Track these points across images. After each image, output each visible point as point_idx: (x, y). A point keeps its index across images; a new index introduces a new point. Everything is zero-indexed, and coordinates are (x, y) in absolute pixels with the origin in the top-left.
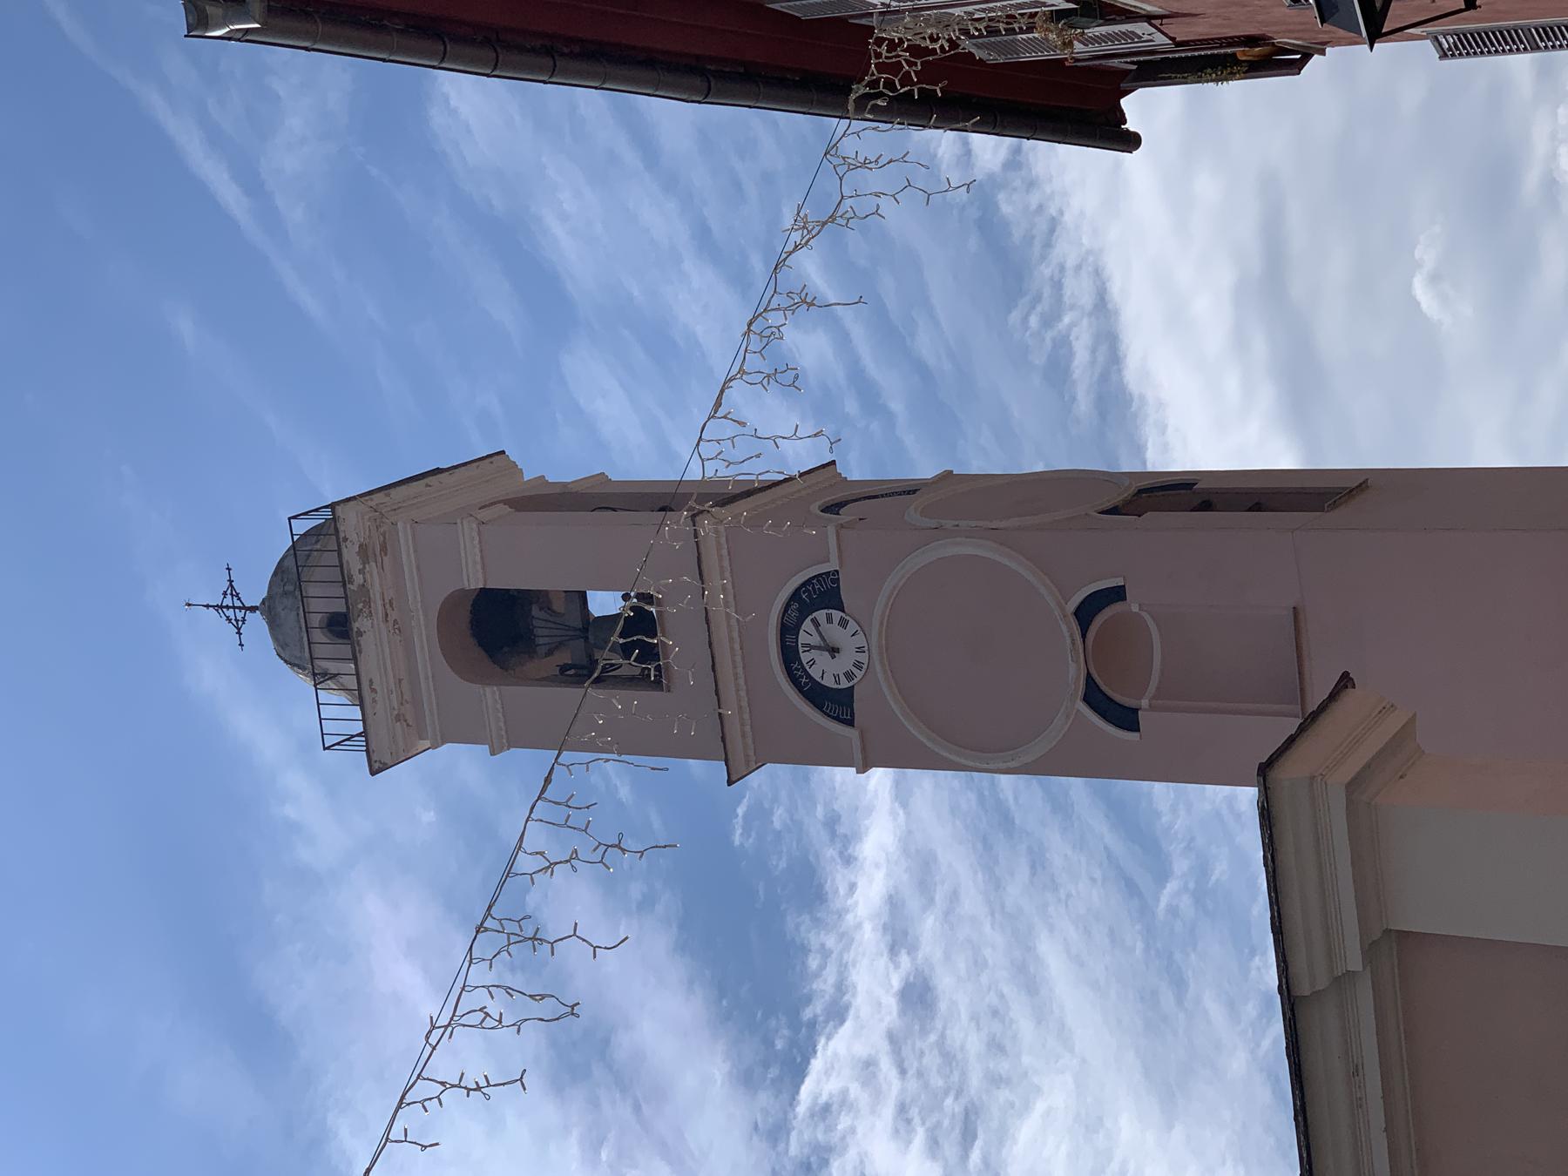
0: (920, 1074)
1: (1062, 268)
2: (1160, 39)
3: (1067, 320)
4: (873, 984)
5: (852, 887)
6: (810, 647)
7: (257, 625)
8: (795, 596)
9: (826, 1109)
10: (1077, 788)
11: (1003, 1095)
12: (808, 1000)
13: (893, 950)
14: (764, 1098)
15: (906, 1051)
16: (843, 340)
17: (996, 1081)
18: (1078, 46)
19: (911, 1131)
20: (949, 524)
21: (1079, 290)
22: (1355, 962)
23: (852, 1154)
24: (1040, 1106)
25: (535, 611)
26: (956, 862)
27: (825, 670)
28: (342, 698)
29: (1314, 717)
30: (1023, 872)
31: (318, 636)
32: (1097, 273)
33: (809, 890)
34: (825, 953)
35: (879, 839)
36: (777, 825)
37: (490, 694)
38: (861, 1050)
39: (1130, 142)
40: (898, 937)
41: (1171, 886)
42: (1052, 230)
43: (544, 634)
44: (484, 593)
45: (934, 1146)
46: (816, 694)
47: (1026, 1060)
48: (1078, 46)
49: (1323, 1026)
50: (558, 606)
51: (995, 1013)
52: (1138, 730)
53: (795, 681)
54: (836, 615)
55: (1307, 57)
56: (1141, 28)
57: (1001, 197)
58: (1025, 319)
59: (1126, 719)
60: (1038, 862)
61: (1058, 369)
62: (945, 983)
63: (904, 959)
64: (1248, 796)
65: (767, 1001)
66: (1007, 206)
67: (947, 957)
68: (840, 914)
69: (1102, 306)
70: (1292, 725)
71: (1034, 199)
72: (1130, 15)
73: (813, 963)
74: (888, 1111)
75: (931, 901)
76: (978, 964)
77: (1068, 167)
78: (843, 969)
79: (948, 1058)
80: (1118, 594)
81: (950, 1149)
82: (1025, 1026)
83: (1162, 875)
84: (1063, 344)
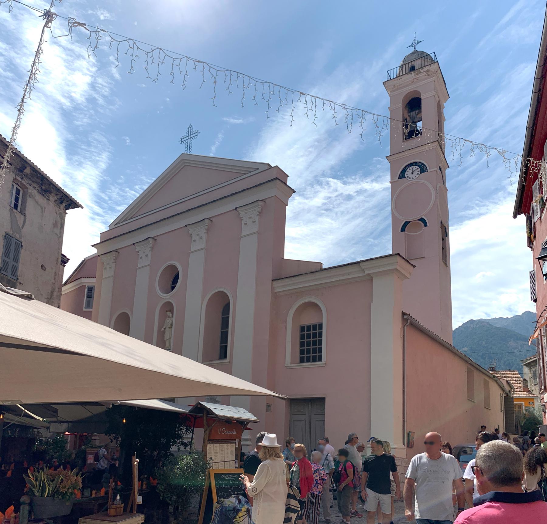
0: (336, 200)
1: (488, 206)
2: (536, 219)
3: (478, 208)
4: (351, 189)
5: (367, 182)
6: (413, 168)
7: (412, 50)
8: (423, 164)
9: (328, 184)
10: (390, 221)
11: (334, 215)
12: (347, 177)
13: (357, 192)
14: (329, 172)
15: (340, 197)
16: (474, 164)
17: (336, 214)
18: (535, 204)
19: (326, 199)
20: (438, 192)
21: (483, 210)
22: (367, 272)
23: (321, 189)
24: (333, 222)
25: (417, 111)
26: (374, 201)
27: (409, 172)
28: (398, 73)
29: (408, 262)
30: (373, 214)
31: (410, 64)
32: (487, 213)
33: (366, 174)
34: (355, 179)
35: (377, 186)
36: (378, 166)
37: (401, 105)
38: (339, 188)
39: (515, 217)
40: (359, 192)
41: (372, 240)
42: (495, 203)
43: (413, 114)
44: (421, 99)
45: (324, 204)
46: (404, 171)
47: (340, 218)
48: (535, 204)
49: (355, 268)
50: (419, 116)
51: (348, 212)
52: (401, 231)
53: (406, 166)
54: (419, 173)
55: (531, 248)
56: (539, 216)
57: (502, 192)
58: (477, 200)
59: (403, 230)
60: (375, 216)
61: (467, 208)
62: (352, 202)
63: (355, 194)
64: (391, 253)
65: (346, 170)
66: (500, 194)
67: (357, 202)
68: (362, 181)
69: (480, 215)
70: (406, 259)
71: (501, 199)
72: (541, 213)
73: (353, 177)
74: (329, 195)
75: (366, 197)
76: (356, 208)
77: (511, 203)
78: (352, 183)
79: (339, 205)
80: (426, 225)
81: (324, 207)
82: (347, 217)
83: (374, 238)
84: (473, 208)
